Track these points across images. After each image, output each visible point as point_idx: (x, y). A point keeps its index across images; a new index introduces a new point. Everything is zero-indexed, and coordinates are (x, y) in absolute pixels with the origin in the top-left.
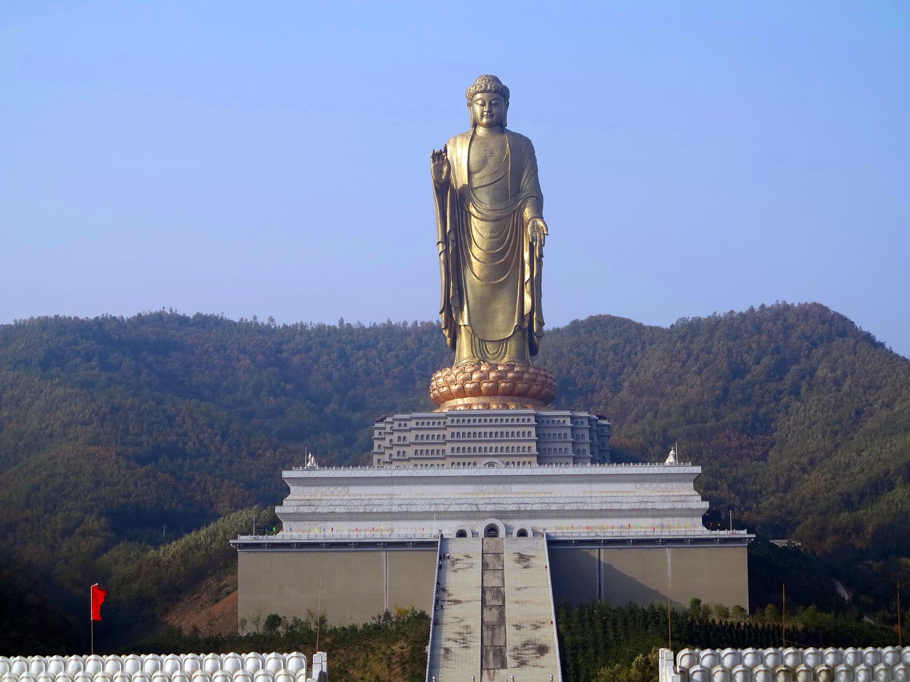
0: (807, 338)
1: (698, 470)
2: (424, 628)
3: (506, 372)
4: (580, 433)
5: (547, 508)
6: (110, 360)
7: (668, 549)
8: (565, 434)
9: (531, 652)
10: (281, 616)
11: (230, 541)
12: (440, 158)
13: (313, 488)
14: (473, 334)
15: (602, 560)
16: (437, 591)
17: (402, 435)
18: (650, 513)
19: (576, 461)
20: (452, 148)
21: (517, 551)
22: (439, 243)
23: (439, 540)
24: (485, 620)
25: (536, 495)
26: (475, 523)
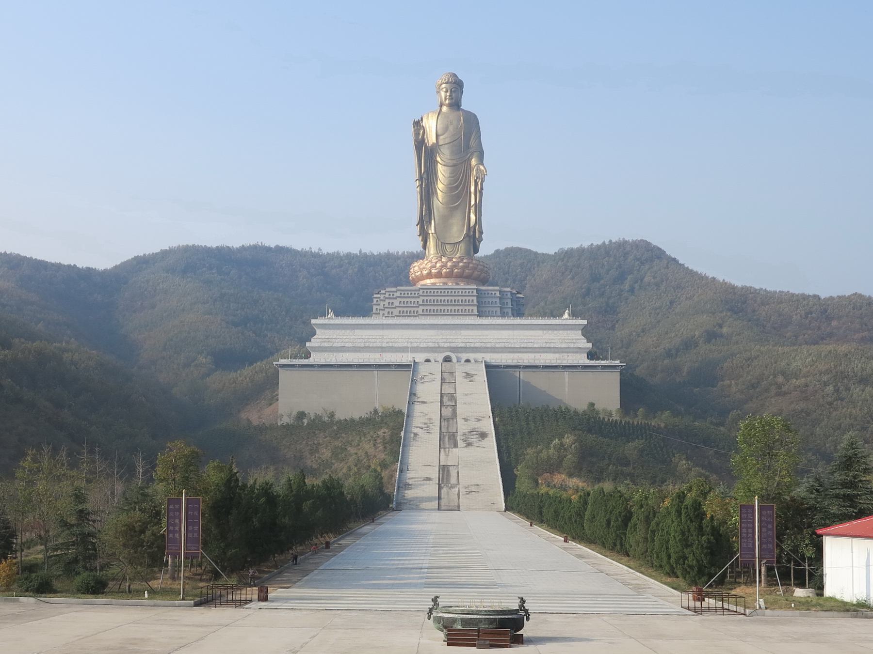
0: (638, 260)
1: (585, 322)
2: (400, 420)
3: (459, 262)
4: (505, 301)
5: (485, 346)
6: (223, 269)
7: (566, 372)
8: (496, 302)
9: (475, 437)
10: (306, 413)
11: (274, 363)
12: (418, 124)
13: (332, 331)
14: (438, 239)
15: (521, 378)
16: (410, 395)
17: (391, 301)
18: (553, 350)
19: (503, 315)
20: (426, 120)
21: (466, 371)
22: (417, 180)
23: (412, 364)
24: (443, 415)
25: (478, 337)
26: (436, 354)
